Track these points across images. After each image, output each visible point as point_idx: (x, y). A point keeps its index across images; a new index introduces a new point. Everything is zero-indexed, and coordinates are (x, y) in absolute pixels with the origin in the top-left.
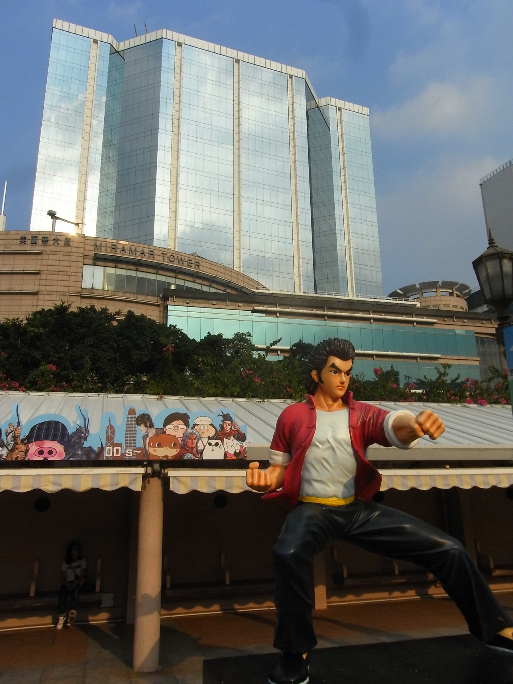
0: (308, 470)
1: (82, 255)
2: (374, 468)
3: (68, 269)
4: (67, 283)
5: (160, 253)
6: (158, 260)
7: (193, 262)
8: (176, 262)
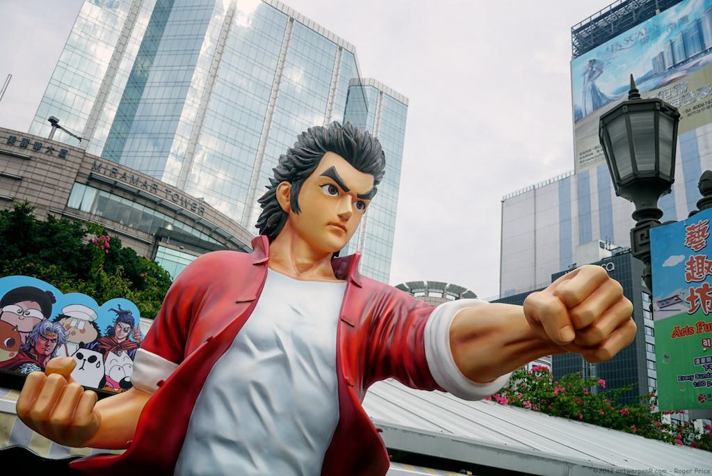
0: (209, 410)
1: (76, 171)
2: (651, 207)
3: (55, 182)
4: (50, 197)
5: (164, 189)
6: (159, 196)
7: (198, 207)
8: (180, 202)
